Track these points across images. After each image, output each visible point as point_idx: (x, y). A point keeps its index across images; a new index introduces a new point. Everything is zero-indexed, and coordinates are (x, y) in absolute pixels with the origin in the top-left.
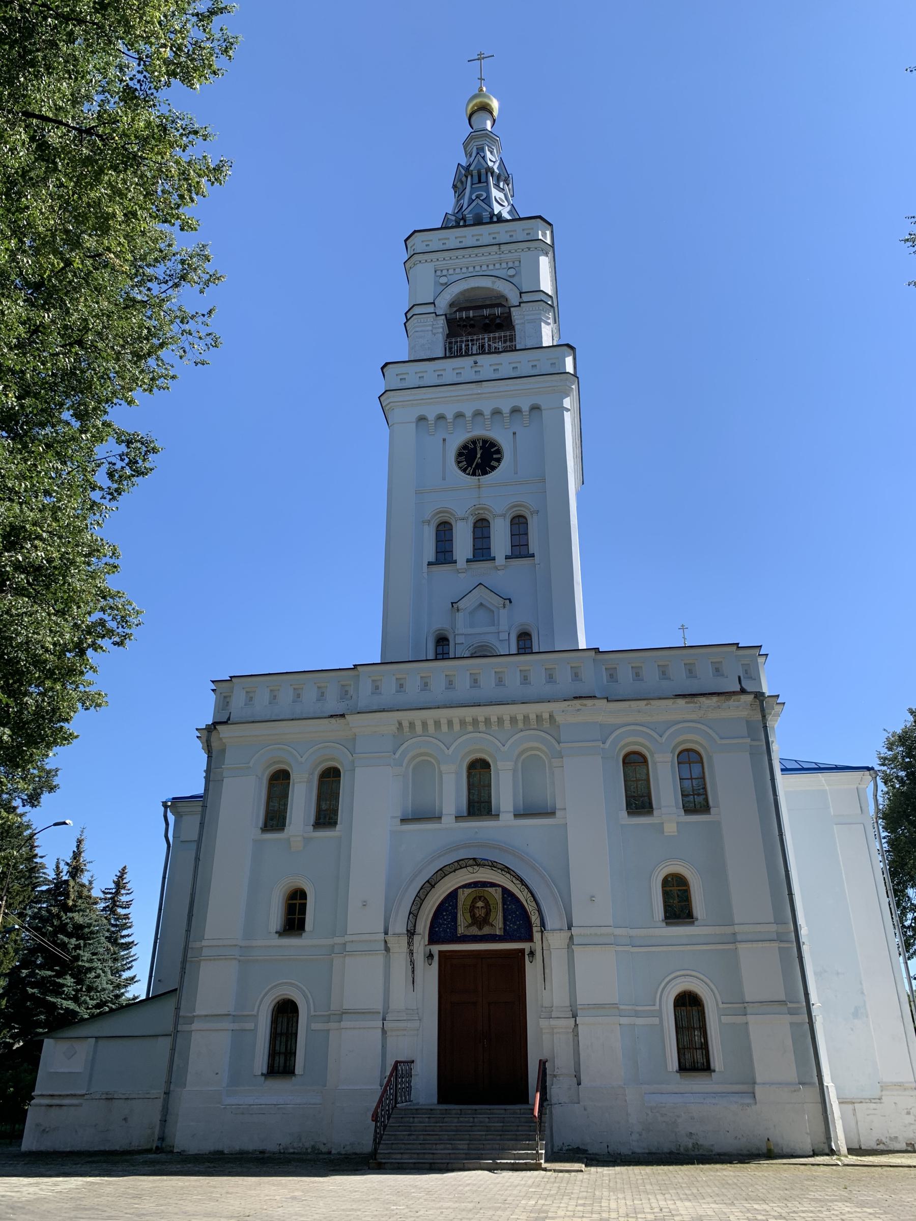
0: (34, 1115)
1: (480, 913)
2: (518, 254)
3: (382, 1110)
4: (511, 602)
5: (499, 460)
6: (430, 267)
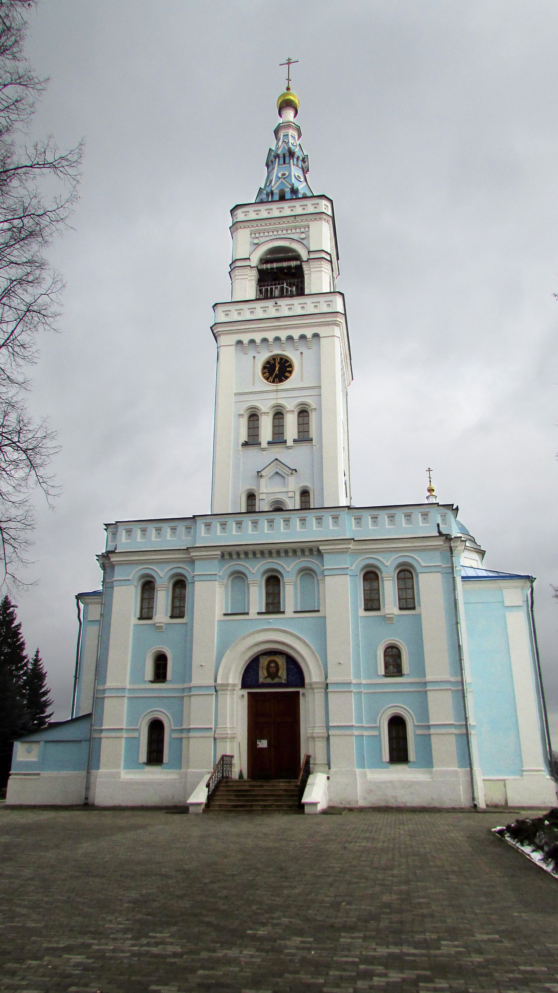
0: (13, 784)
1: (273, 670)
2: (308, 223)
3: (213, 783)
4: (296, 471)
5: (291, 372)
6: (247, 232)
